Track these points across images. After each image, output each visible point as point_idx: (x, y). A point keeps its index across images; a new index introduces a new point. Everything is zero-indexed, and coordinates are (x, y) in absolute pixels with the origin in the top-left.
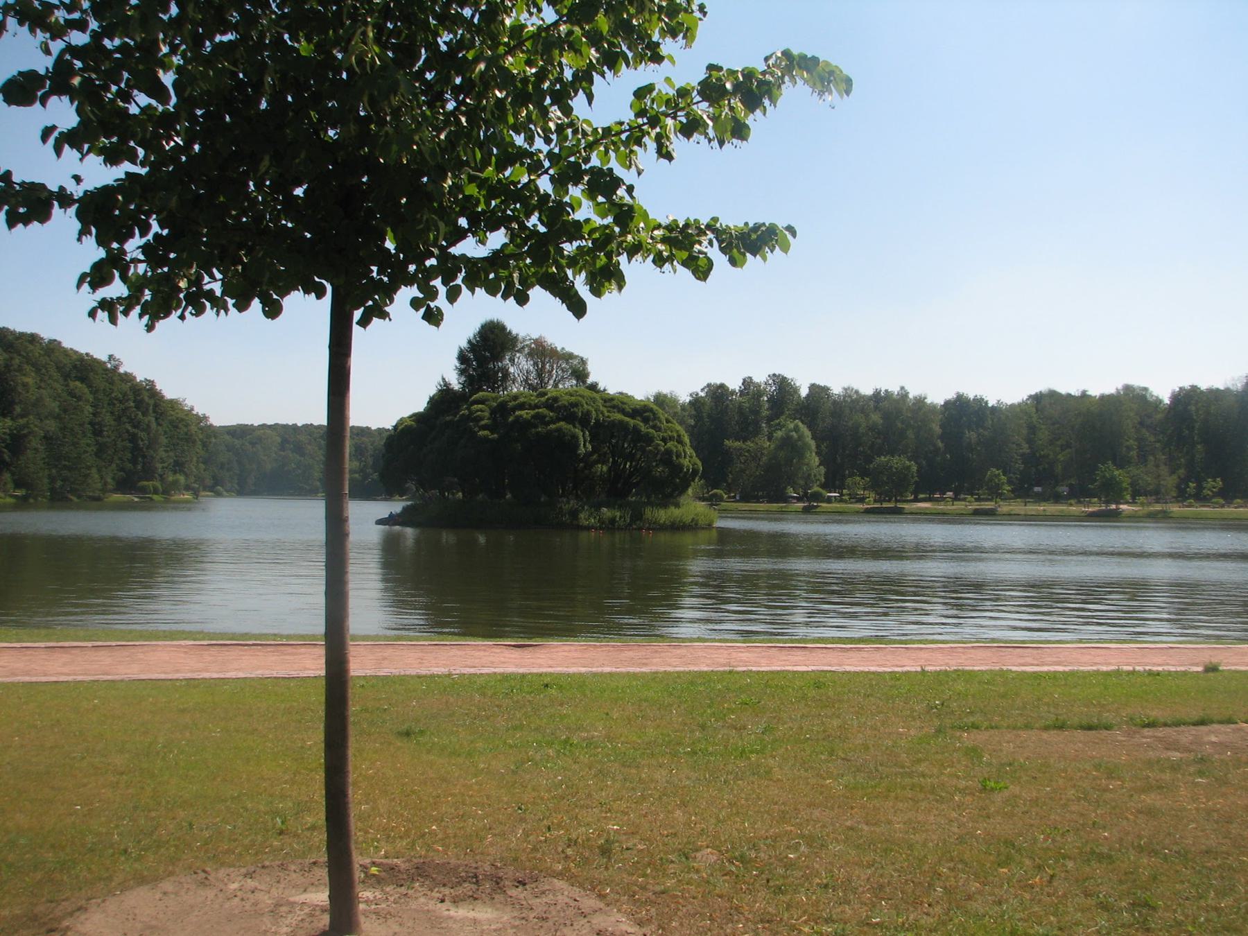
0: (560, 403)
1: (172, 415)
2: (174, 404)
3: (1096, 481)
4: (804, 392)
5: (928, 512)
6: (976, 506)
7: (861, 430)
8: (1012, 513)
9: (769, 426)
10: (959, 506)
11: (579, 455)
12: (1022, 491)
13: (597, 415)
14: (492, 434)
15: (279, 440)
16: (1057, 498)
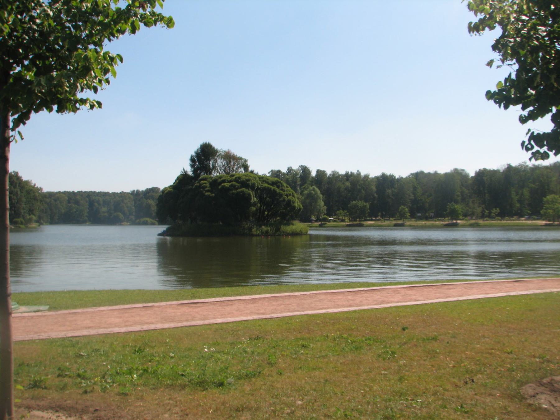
0: (242, 180)
1: (27, 188)
2: (27, 183)
3: (447, 210)
4: (314, 174)
5: (375, 225)
6: (394, 222)
7: (341, 190)
8: (412, 225)
9: (301, 189)
10: (387, 223)
11: (251, 203)
12: (413, 216)
13: (258, 185)
14: (212, 194)
15: (67, 198)
16: (427, 218)
